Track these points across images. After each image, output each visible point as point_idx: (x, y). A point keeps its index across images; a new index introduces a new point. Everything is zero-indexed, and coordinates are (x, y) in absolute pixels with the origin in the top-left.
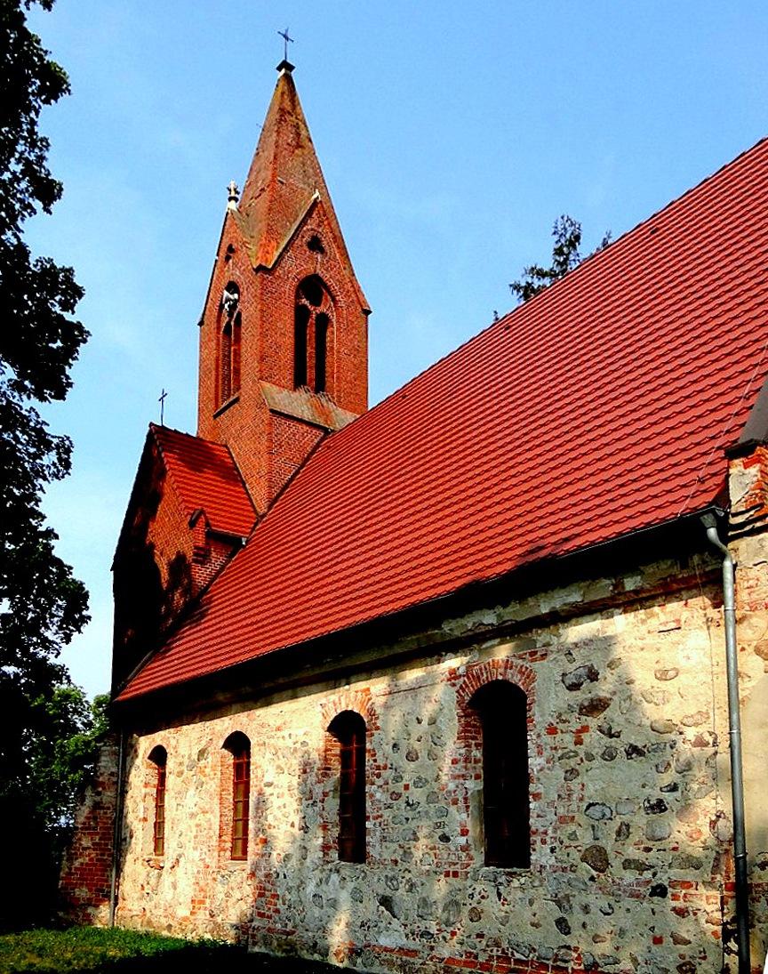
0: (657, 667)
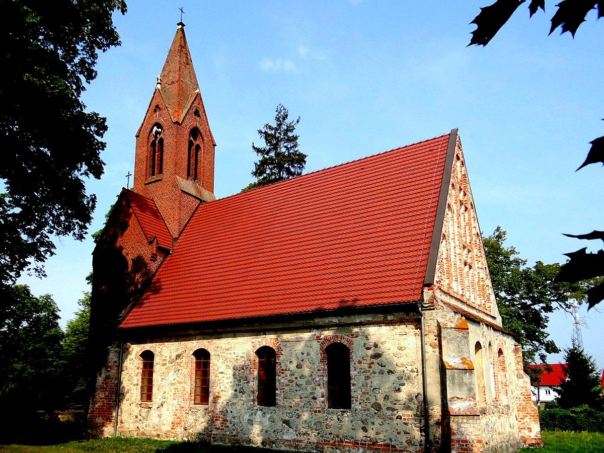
0: (399, 346)
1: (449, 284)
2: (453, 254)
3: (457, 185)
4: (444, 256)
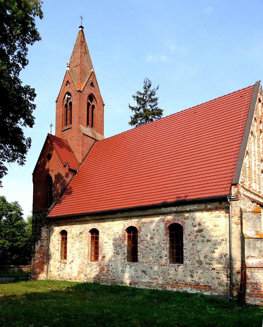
0: (214, 224)
1: (250, 185)
2: (253, 165)
3: (258, 119)
4: (247, 166)
